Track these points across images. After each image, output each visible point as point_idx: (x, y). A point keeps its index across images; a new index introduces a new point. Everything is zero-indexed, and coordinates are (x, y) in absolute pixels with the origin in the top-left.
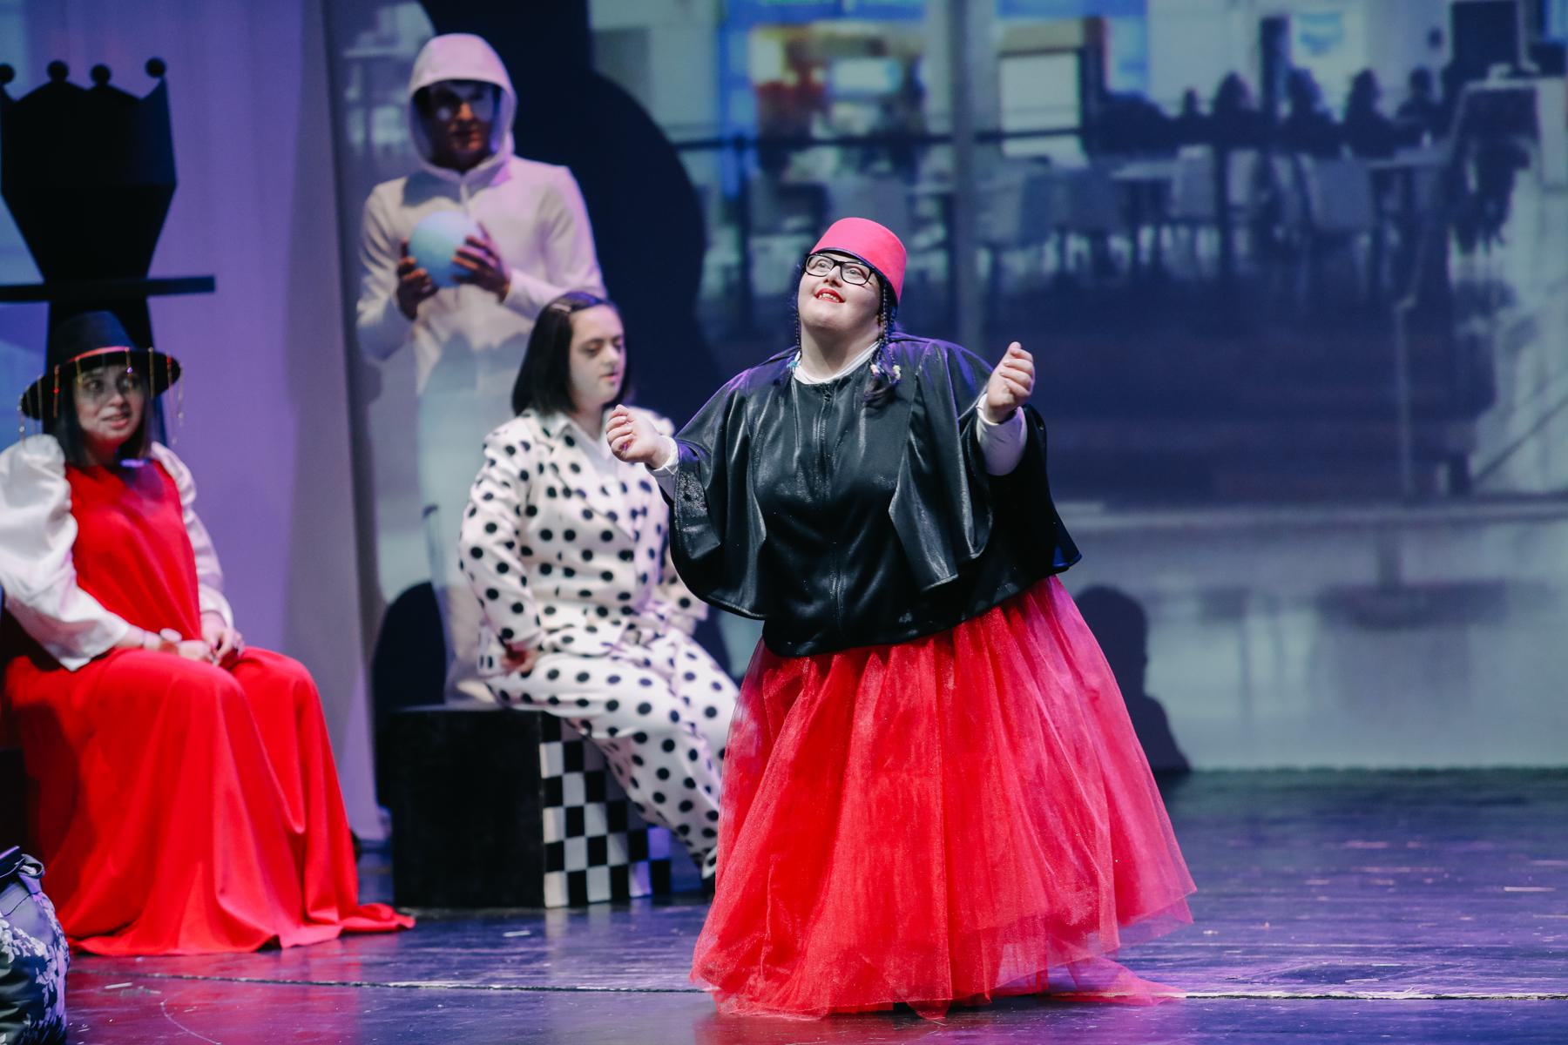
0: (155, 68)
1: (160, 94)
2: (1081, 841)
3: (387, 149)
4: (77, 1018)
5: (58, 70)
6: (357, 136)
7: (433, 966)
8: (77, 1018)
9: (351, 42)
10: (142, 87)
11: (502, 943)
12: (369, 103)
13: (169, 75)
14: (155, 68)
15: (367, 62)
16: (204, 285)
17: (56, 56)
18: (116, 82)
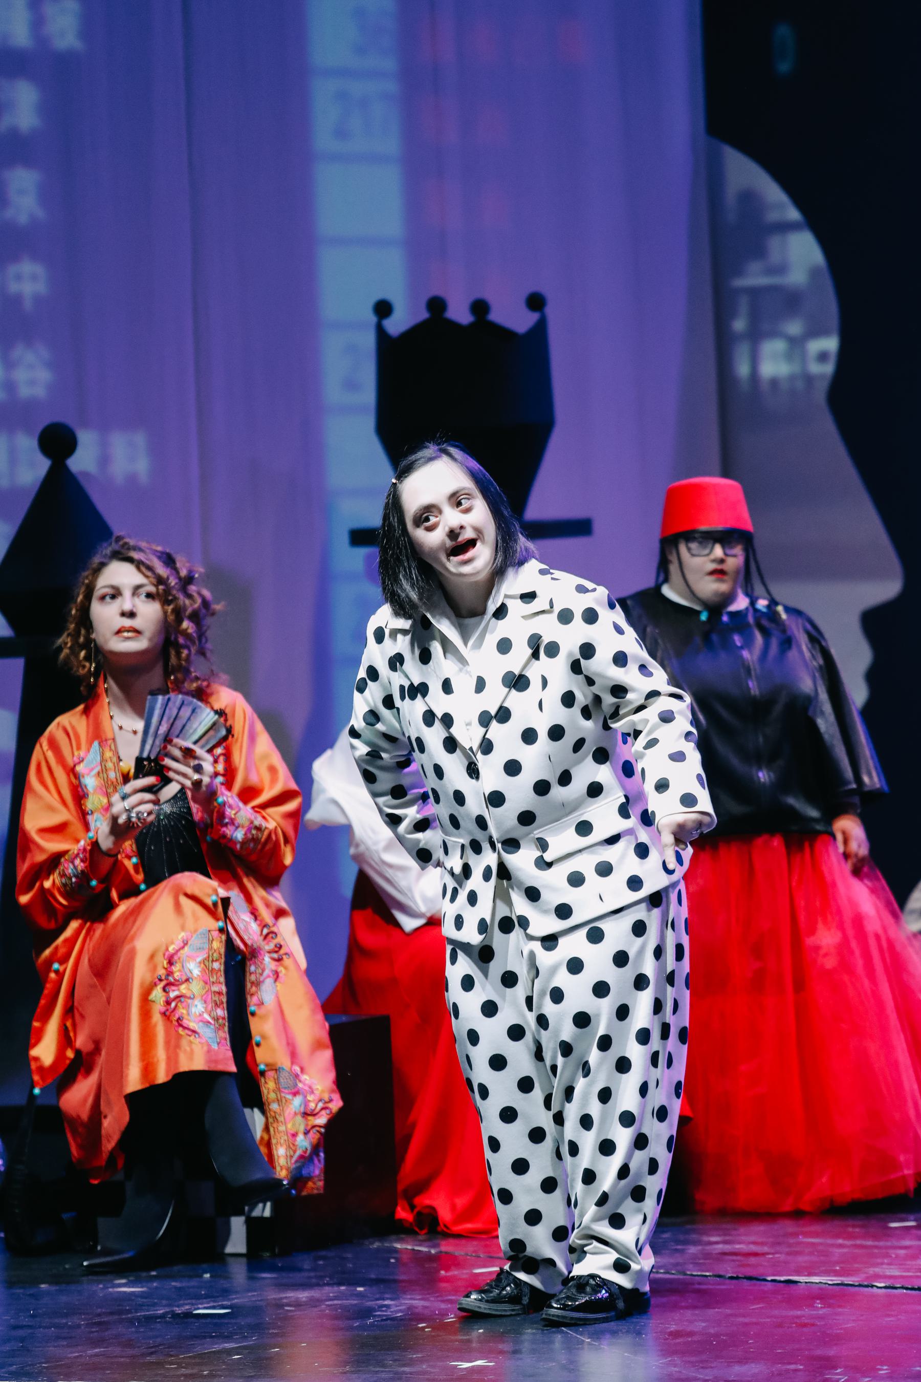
0: (536, 302)
1: (540, 329)
2: (854, 944)
3: (774, 382)
4: (443, 1306)
5: (437, 305)
6: (743, 369)
7: (814, 1258)
8: (443, 1306)
9: (739, 272)
10: (519, 320)
11: (890, 1234)
12: (756, 336)
13: (549, 310)
14: (536, 302)
15: (755, 293)
16: (580, 528)
17: (436, 291)
18: (496, 316)
